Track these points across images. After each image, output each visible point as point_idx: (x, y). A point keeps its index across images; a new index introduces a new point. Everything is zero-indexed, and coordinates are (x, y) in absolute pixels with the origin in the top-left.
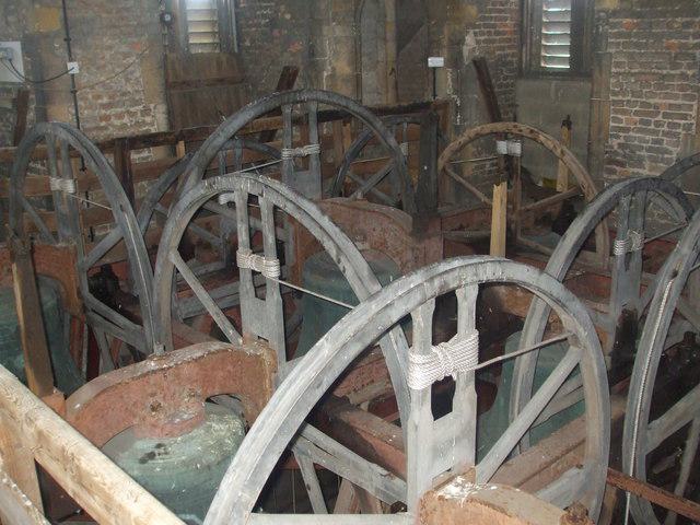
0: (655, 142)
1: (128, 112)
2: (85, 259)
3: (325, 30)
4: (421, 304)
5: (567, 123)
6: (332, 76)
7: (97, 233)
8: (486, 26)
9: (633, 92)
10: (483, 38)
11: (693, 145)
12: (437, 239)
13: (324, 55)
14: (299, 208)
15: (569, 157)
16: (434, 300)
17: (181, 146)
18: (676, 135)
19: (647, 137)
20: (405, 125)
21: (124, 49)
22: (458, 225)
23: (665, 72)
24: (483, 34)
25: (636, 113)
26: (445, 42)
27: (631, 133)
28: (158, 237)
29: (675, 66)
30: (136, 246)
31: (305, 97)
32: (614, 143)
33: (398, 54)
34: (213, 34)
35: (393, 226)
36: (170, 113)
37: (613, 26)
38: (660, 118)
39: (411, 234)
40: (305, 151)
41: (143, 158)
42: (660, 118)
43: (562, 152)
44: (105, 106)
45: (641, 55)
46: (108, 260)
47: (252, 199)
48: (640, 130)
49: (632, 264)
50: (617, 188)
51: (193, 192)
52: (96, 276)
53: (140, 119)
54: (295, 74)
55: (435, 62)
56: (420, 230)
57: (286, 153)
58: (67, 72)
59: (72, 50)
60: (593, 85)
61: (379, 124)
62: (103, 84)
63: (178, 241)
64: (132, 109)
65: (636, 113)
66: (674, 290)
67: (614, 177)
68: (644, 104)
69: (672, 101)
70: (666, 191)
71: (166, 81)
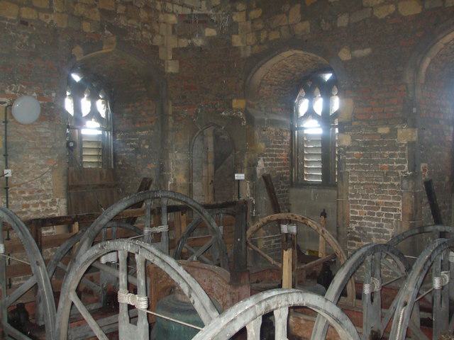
0: (378, 225)
1: (41, 203)
2: (7, 299)
3: (170, 155)
4: (253, 319)
5: (324, 214)
6: (174, 184)
7: (13, 283)
8: (271, 155)
9: (363, 195)
10: (268, 163)
11: (401, 226)
12: (246, 286)
13: (169, 170)
14: (163, 261)
15: (327, 234)
16: (261, 317)
17: (76, 226)
18: (390, 221)
19: (373, 223)
20: (222, 215)
21: (42, 162)
22: (255, 280)
23: (381, 183)
24: (268, 160)
25: (366, 208)
26: (245, 164)
27: (363, 221)
28: (60, 286)
29: (387, 179)
30: (46, 289)
31: (160, 194)
32: (353, 226)
33: (215, 170)
34: (98, 156)
35: (221, 275)
36: (69, 205)
37: (348, 156)
38: (380, 211)
39: (230, 284)
40: (158, 229)
41: (49, 233)
42: (380, 211)
43: (323, 231)
44: (25, 198)
45: (366, 173)
46: (20, 301)
47: (130, 258)
48: (369, 219)
49: (375, 300)
50: (363, 250)
51: (86, 255)
52: (12, 312)
53: (49, 208)
54: (151, 182)
55: (240, 176)
56: (235, 280)
57: (146, 231)
58: (4, 175)
59: (8, 161)
60: (338, 190)
61: (206, 213)
62: (26, 184)
63: (76, 285)
64: (44, 201)
65: (366, 208)
66: (406, 315)
67: (354, 248)
68: (370, 203)
69: (387, 201)
70: (393, 253)
71: (68, 184)
